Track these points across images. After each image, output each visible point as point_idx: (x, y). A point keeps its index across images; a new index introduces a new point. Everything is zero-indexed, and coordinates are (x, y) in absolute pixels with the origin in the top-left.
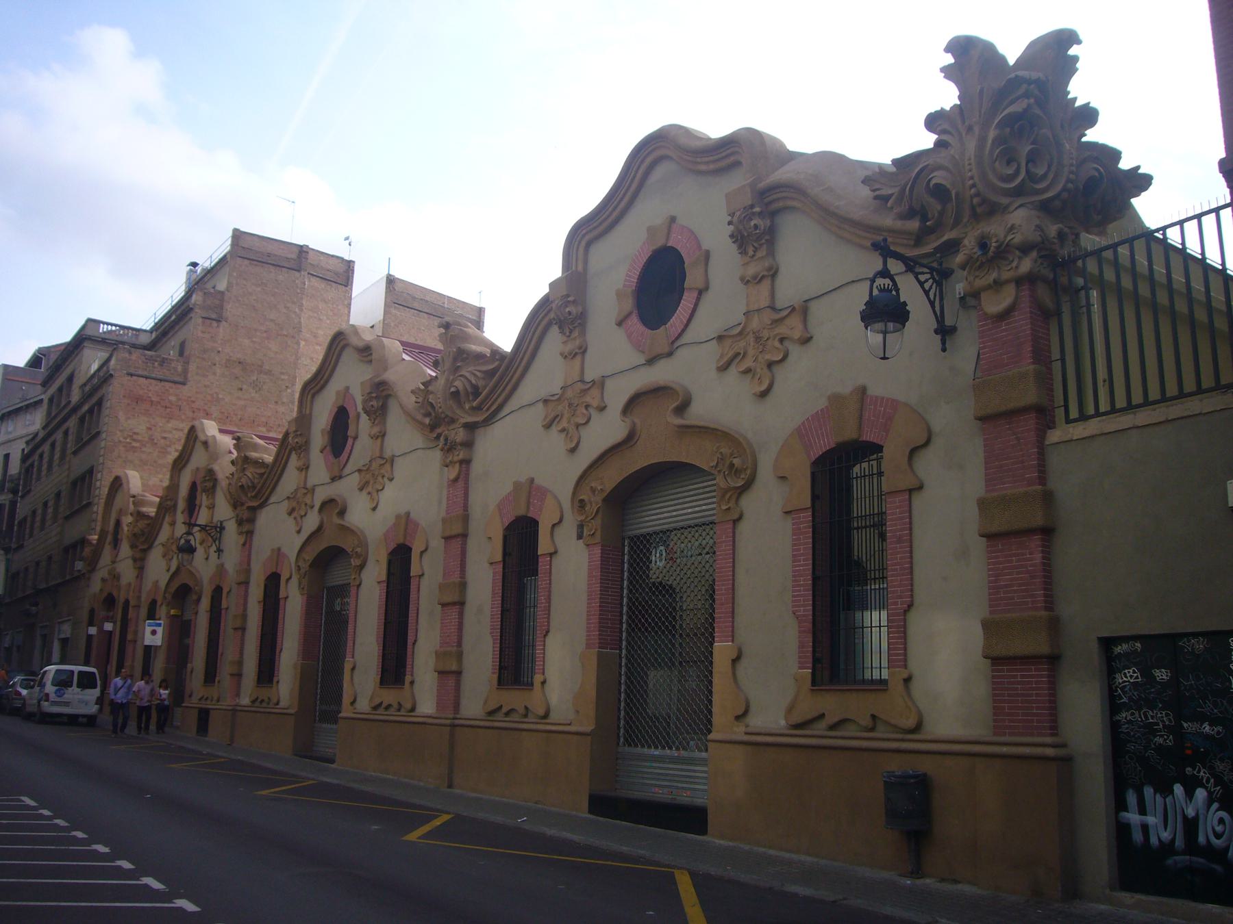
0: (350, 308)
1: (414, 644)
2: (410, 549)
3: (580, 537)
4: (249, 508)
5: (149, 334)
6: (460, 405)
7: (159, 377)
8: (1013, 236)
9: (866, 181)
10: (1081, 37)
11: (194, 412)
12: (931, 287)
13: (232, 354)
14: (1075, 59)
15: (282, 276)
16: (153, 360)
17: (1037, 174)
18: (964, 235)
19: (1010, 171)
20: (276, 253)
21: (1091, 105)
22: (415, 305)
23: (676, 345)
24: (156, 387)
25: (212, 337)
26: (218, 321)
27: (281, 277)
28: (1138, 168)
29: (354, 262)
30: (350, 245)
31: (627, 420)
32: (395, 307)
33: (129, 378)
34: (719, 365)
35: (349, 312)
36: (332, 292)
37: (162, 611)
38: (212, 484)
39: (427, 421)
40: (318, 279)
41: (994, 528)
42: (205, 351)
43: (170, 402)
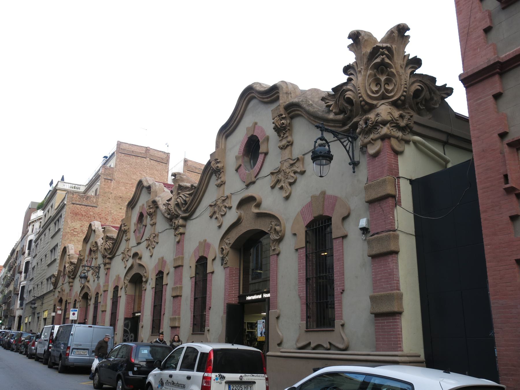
0: (168, 173)
1: (164, 315)
2: (163, 273)
3: (222, 265)
4: (109, 258)
5: (85, 187)
6: (180, 209)
7: (85, 204)
8: (378, 118)
9: (323, 99)
10: (409, 27)
11: (100, 219)
12: (347, 144)
13: (117, 194)
14: (408, 37)
15: (139, 160)
16: (83, 197)
17: (389, 90)
18: (360, 120)
19: (376, 89)
20: (136, 151)
21: (417, 57)
22: (196, 171)
23: (258, 177)
24: (84, 208)
25: (108, 187)
26: (111, 180)
27: (138, 161)
28: (446, 85)
29: (170, 153)
30: (168, 146)
31: (238, 211)
32: (188, 172)
33: (73, 205)
34: (271, 185)
35: (168, 175)
36: (160, 167)
37: (78, 305)
38: (96, 248)
39: (169, 216)
40: (154, 161)
41: (374, 253)
42: (105, 193)
43: (90, 215)
